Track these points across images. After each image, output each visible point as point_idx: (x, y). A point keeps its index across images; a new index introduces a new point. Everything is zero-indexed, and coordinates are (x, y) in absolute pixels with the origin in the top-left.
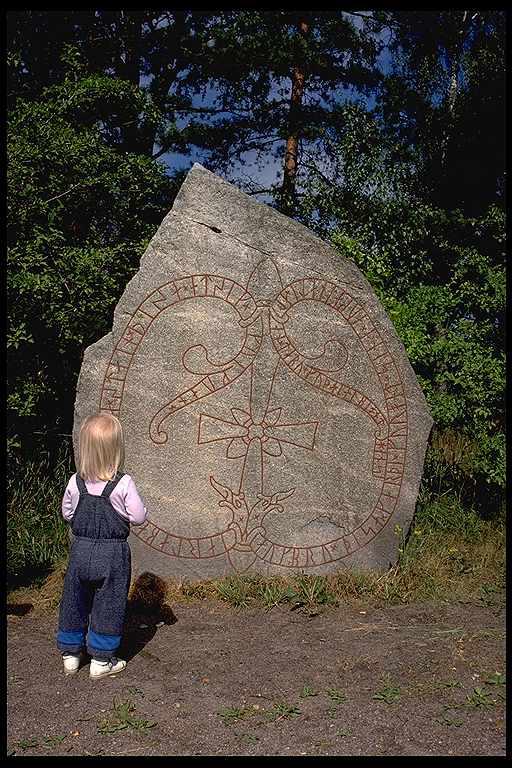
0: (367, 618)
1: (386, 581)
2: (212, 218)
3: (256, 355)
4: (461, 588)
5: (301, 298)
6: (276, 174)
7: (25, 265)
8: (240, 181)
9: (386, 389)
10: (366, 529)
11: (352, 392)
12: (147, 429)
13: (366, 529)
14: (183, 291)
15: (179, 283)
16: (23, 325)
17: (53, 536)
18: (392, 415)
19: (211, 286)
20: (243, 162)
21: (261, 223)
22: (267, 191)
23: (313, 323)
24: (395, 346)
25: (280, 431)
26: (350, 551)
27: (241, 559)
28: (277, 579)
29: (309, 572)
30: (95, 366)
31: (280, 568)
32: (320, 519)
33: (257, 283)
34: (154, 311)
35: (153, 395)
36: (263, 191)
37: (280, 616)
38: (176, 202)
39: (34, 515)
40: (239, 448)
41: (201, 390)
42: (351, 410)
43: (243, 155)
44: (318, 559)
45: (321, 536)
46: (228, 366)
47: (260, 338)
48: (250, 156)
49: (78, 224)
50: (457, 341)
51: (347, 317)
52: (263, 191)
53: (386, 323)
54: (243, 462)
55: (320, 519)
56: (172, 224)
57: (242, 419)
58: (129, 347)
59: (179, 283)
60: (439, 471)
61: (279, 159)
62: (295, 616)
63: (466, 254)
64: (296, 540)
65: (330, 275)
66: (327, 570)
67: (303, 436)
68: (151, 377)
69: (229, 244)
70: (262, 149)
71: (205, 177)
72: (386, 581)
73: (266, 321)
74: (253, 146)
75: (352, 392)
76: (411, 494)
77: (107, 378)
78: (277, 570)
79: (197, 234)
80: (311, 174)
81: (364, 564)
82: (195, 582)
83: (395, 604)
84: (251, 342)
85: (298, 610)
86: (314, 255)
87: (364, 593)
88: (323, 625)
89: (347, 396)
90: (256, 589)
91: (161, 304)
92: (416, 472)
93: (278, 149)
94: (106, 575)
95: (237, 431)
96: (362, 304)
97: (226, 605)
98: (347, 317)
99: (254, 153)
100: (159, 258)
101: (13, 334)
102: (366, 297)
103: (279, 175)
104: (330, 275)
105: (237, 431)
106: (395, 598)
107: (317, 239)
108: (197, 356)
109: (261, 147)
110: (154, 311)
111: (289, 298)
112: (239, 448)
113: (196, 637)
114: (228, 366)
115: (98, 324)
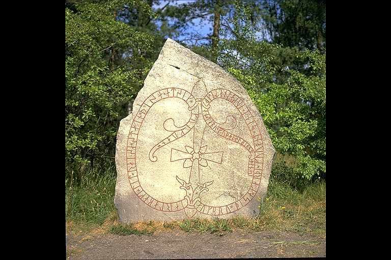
0: (245, 237)
1: (255, 222)
2: (175, 62)
3: (196, 123)
4: (288, 224)
5: (216, 97)
6: (209, 29)
7: (91, 82)
8: (192, 33)
9: (254, 137)
10: (245, 198)
11: (239, 138)
12: (148, 155)
13: (245, 198)
14: (164, 94)
15: (161, 92)
16: (91, 108)
17: (106, 203)
18: (257, 148)
19: (176, 92)
20: (193, 24)
21: (197, 65)
22: (205, 38)
23: (219, 109)
24: (257, 118)
25: (206, 156)
26: (238, 208)
27: (190, 212)
28: (206, 220)
29: (220, 217)
30: (125, 127)
31: (207, 215)
32: (225, 194)
33: (196, 91)
34: (150, 104)
35: (149, 140)
36: (204, 38)
37: (206, 236)
38: (160, 56)
39: (98, 193)
40: (188, 163)
41: (172, 138)
42: (238, 146)
43: (194, 21)
44: (224, 211)
45: (226, 201)
46: (183, 128)
47: (197, 115)
48: (196, 21)
49: (113, 58)
50: (288, 113)
51: (236, 105)
52: (204, 38)
53: (254, 108)
54: (190, 171)
55: (225, 194)
56: (158, 66)
57: (190, 150)
58: (140, 120)
59: (161, 92)
60: (281, 171)
61: (211, 22)
62: (213, 236)
63: (294, 73)
64: (214, 203)
65: (228, 87)
66: (229, 216)
67: (217, 158)
68: (149, 133)
69: (184, 75)
70: (202, 17)
71: (173, 45)
72: (255, 222)
73: (200, 108)
74: (199, 16)
75: (239, 138)
76: (265, 183)
77: (131, 133)
78: (205, 217)
79: (170, 70)
80: (227, 29)
81: (245, 213)
82: (169, 222)
83: (258, 231)
84: (194, 117)
85: (215, 234)
86: (221, 78)
87: (244, 227)
88: (225, 240)
89: (236, 139)
90: (197, 223)
91: (153, 101)
92: (267, 172)
93: (211, 18)
94: (125, 221)
95: (188, 156)
96: (243, 100)
97: (183, 232)
98: (236, 105)
99: (199, 19)
100: (151, 84)
101: (85, 112)
102: (244, 97)
103: (211, 29)
104: (228, 87)
105: (188, 156)
106: (257, 229)
107: (223, 71)
108: (170, 123)
109: (202, 17)
110: (150, 104)
111: (209, 97)
112: (188, 163)
113: (170, 245)
114: (183, 128)
115: (124, 109)
